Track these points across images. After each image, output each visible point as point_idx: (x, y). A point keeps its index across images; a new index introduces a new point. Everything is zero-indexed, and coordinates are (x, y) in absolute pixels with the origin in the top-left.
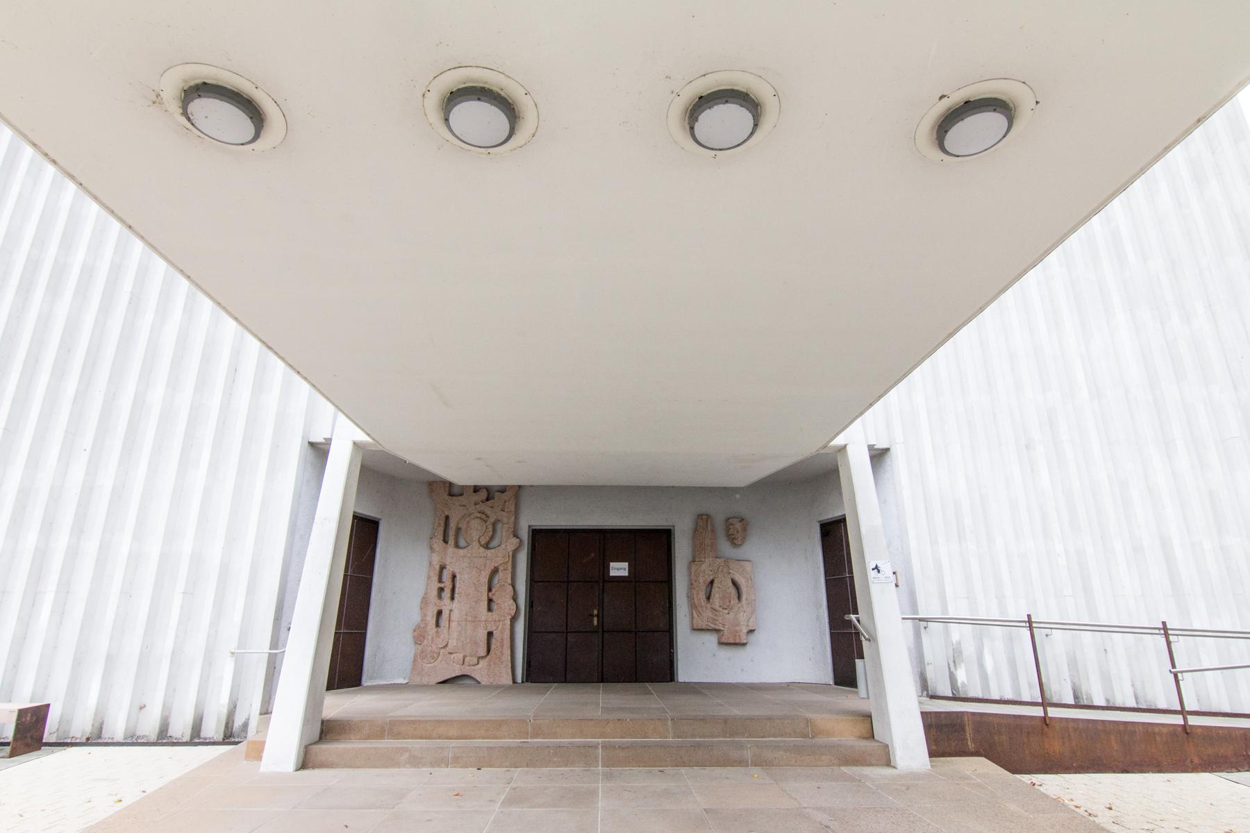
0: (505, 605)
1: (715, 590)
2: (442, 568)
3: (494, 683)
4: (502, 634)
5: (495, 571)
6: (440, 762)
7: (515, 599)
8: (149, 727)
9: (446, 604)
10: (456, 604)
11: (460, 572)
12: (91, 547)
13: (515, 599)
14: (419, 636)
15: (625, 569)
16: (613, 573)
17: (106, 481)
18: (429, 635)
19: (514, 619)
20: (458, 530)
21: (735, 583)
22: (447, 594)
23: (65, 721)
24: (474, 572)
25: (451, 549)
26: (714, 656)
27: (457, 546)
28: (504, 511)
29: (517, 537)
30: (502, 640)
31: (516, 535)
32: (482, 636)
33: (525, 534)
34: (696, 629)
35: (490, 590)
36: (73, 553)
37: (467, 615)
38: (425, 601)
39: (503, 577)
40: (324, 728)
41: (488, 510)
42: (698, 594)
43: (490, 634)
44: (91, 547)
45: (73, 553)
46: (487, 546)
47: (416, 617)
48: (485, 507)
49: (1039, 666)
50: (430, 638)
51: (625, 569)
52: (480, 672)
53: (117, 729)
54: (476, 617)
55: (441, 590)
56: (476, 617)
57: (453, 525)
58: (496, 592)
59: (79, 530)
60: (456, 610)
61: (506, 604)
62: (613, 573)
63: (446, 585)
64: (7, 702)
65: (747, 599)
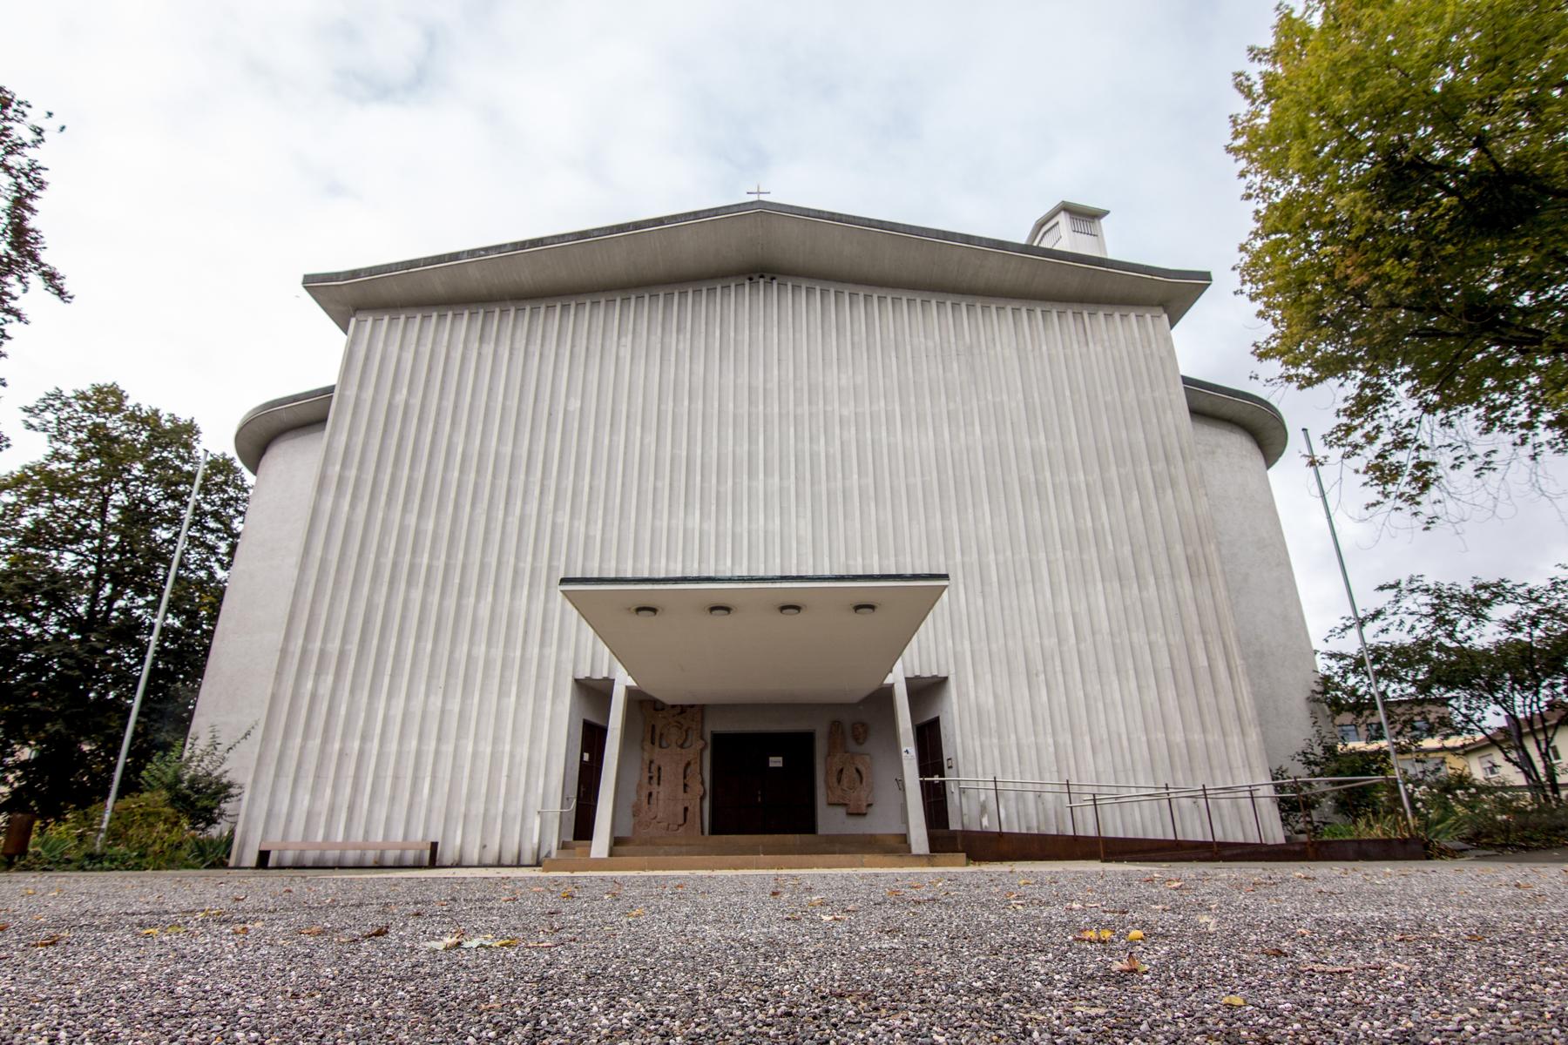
1: (844, 776)
5: (688, 764)
7: (703, 783)
10: (661, 788)
12: (448, 748)
19: (702, 799)
21: (858, 771)
25: (657, 749)
31: (702, 738)
33: (708, 738)
35: (685, 777)
38: (640, 786)
39: (694, 768)
43: (686, 809)
46: (682, 746)
55: (651, 778)
60: (662, 792)
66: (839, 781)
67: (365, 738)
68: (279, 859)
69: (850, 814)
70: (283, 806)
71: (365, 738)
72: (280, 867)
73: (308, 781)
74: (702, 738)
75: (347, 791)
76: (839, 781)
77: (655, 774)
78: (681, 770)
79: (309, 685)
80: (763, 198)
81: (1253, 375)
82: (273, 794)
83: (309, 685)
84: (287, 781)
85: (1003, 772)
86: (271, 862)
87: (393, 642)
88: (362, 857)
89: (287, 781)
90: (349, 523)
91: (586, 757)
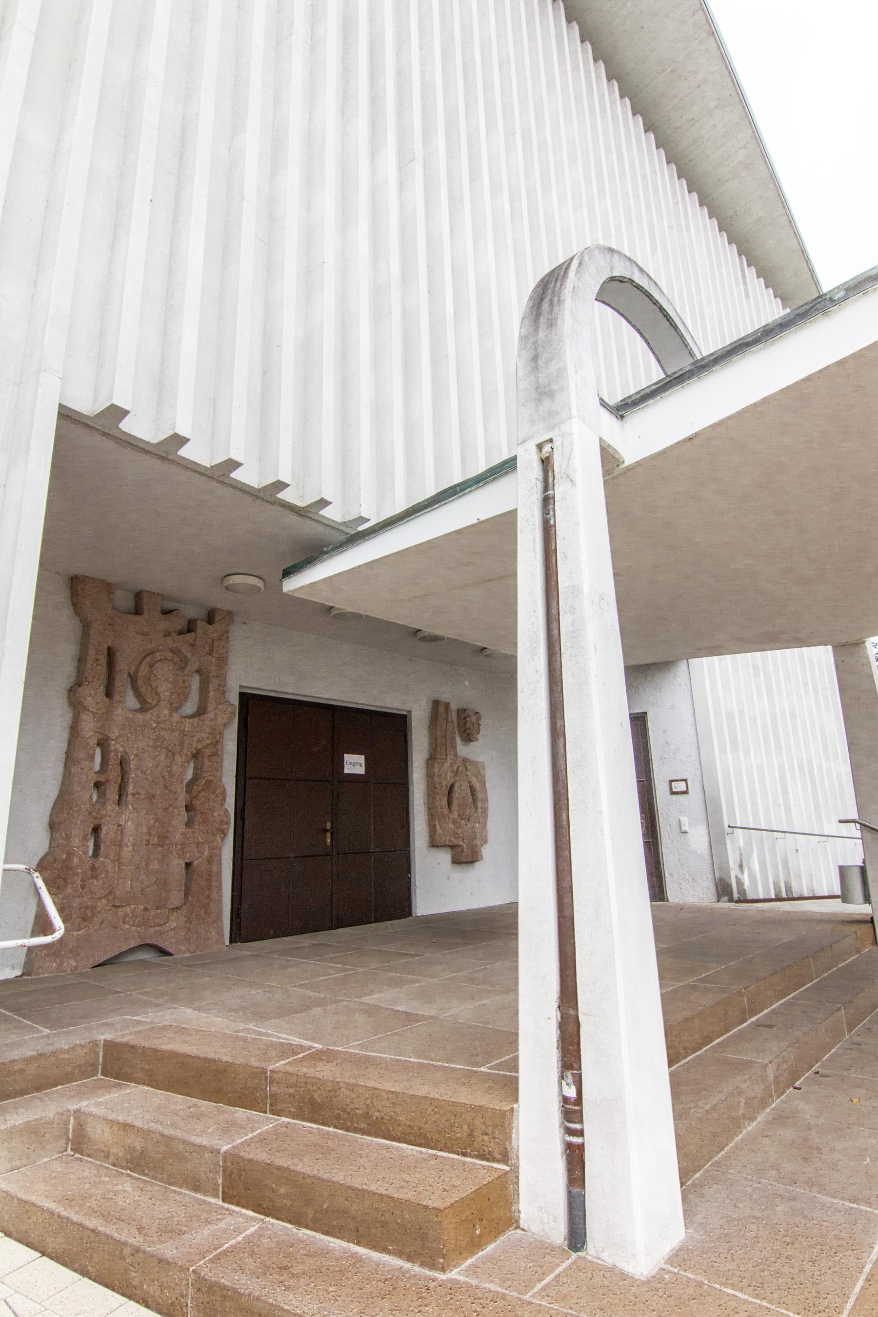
11: (136, 755)
15: (361, 765)
16: (348, 770)
18: (77, 874)
22: (112, 792)
24: (162, 758)
26: (449, 878)
28: (211, 655)
30: (210, 875)
34: (434, 844)
37: (150, 834)
40: (578, 1061)
41: (186, 650)
42: (441, 800)
48: (182, 643)
49: (650, 874)
50: (78, 881)
51: (361, 765)
54: (166, 837)
56: (166, 837)
57: (123, 666)
58: (199, 792)
61: (216, 814)
62: (348, 770)
64: (86, 578)
65: (482, 808)
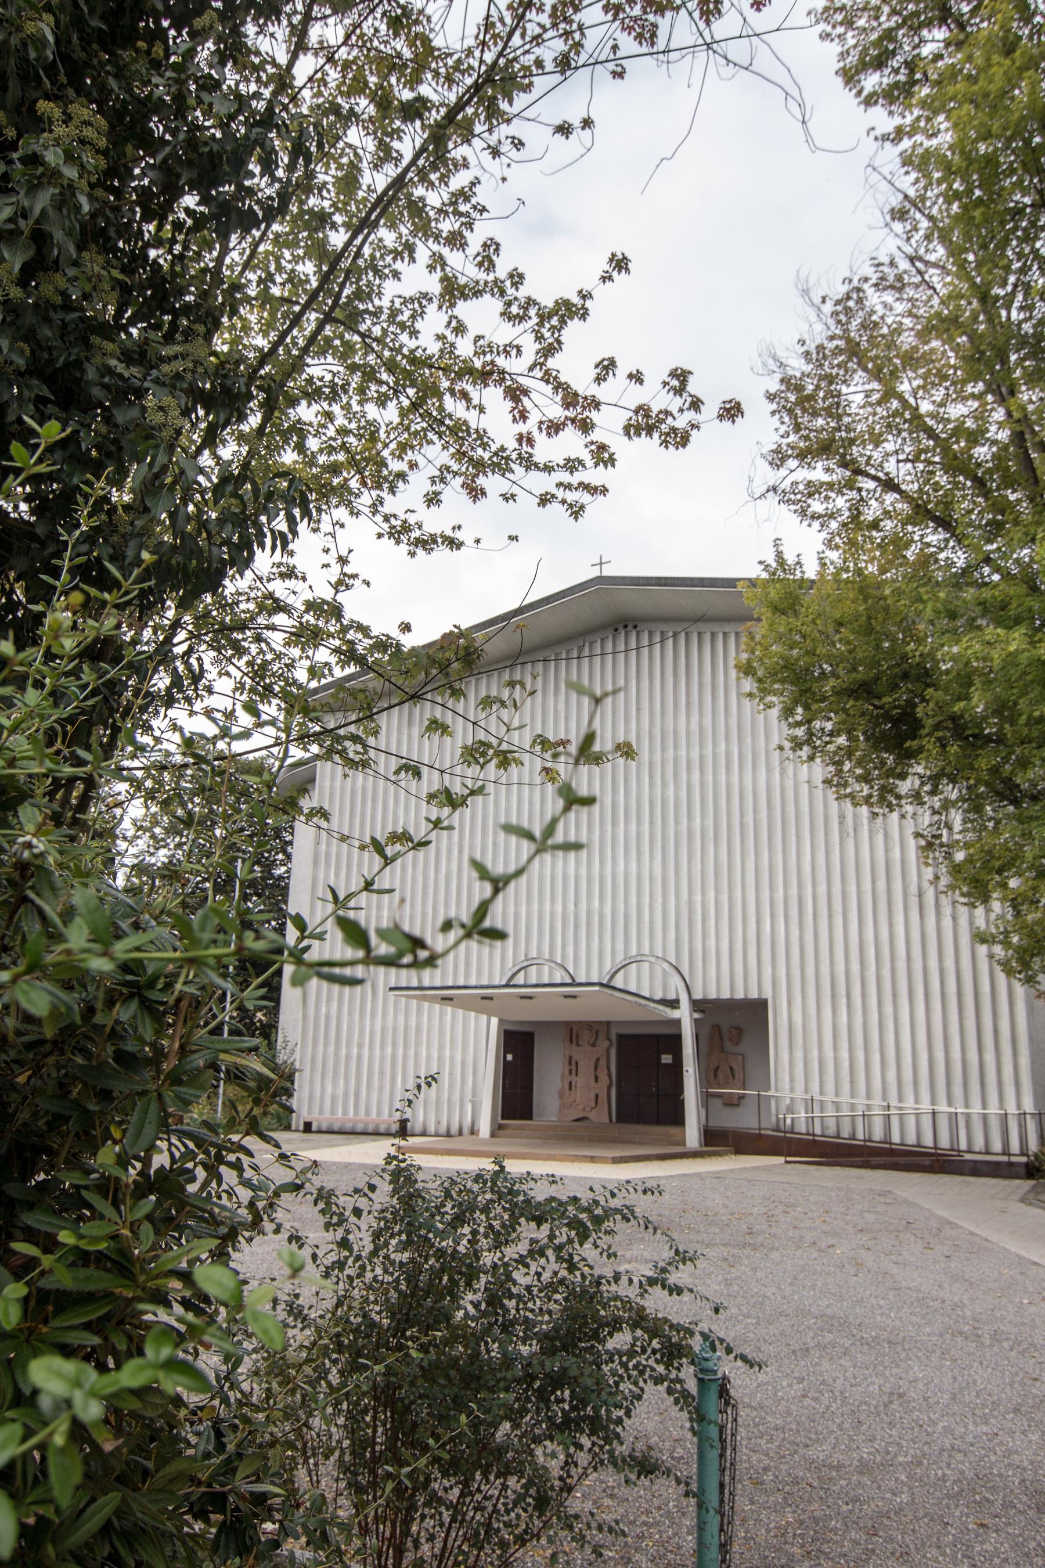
0: (604, 1079)
1: (719, 1072)
2: (571, 1058)
3: (103, 143)
4: (603, 1096)
5: (598, 1060)
6: (534, 1138)
7: (610, 1076)
8: (443, 1130)
9: (573, 1078)
10: (578, 1079)
12: (411, 1053)
13: (610, 1076)
14: (561, 1095)
17: (413, 1023)
19: (609, 1087)
20: (578, 1036)
21: (731, 1068)
23: (413, 1127)
25: (574, 1047)
27: (578, 1045)
29: (564, 424)
31: (609, 1039)
32: (593, 1096)
33: (614, 1038)
35: (596, 1069)
36: (405, 1056)
38: (563, 1076)
39: (603, 1063)
43: (597, 1096)
44: (411, 1053)
45: (405, 1056)
46: (594, 1045)
47: (559, 1085)
52: (593, 1116)
53: (432, 1129)
55: (570, 1071)
59: (406, 1046)
60: (579, 1081)
63: (573, 1066)
66: (716, 1076)
67: (360, 1046)
68: (319, 1126)
69: (726, 1104)
70: (318, 1093)
71: (360, 1046)
72: (320, 1132)
73: (330, 1075)
74: (609, 1039)
75: (353, 1082)
76: (716, 1076)
77: (574, 1067)
78: (592, 1065)
79: (324, 1010)
80: (608, 571)
81: (580, 136)
82: (311, 1083)
83: (324, 1010)
84: (318, 1075)
85: (822, 1093)
86: (314, 1128)
87: (596, 941)
88: (377, 1126)
89: (318, 1075)
90: (577, 878)
91: (509, 1057)
